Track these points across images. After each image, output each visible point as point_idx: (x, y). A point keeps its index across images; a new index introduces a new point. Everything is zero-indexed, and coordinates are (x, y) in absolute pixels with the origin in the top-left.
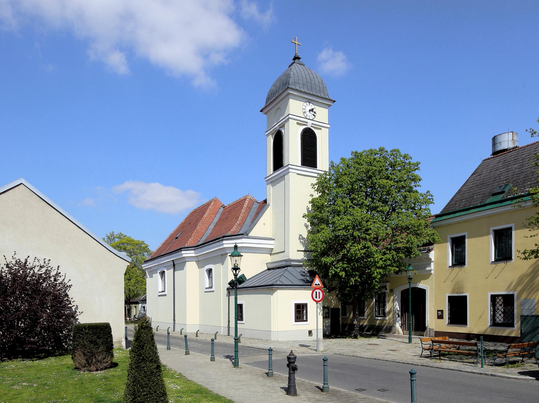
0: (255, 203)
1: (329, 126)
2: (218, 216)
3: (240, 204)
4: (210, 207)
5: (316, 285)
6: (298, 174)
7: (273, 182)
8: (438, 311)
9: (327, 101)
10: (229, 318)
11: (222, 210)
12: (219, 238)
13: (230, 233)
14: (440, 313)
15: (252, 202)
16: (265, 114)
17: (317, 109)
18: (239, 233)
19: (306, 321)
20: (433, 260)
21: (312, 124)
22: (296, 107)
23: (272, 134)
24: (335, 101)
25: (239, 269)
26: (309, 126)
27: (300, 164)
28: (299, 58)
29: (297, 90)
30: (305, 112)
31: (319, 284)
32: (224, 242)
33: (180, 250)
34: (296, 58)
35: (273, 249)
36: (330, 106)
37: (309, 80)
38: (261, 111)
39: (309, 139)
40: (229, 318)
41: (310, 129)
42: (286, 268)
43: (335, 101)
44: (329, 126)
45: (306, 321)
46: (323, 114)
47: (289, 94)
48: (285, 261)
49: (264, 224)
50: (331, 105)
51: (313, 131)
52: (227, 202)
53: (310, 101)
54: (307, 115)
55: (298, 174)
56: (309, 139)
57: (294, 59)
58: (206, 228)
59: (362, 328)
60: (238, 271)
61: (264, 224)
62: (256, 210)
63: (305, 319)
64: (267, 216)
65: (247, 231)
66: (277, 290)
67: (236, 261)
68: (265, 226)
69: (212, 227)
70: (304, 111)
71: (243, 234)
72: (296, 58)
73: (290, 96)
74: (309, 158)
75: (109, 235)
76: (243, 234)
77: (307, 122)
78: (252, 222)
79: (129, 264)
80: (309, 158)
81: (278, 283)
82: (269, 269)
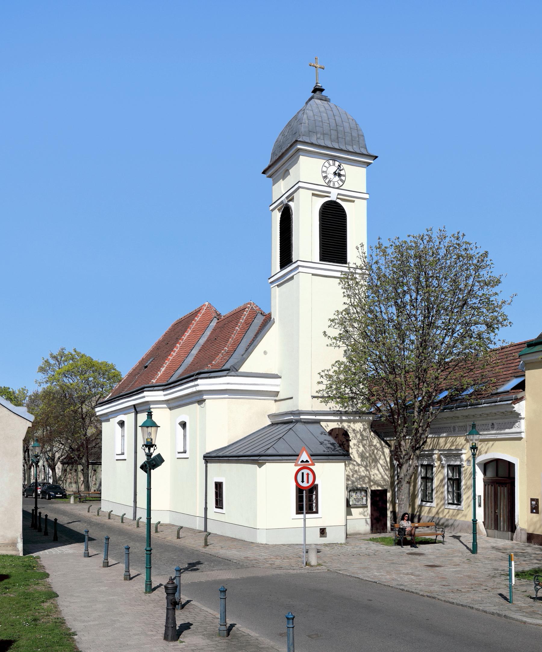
0: (259, 316)
1: (367, 196)
2: (208, 333)
3: (237, 315)
4: (200, 315)
5: (302, 461)
6: (313, 275)
7: (282, 282)
8: (532, 500)
9: (366, 158)
10: (206, 503)
11: (215, 321)
12: (193, 376)
13: (209, 368)
14: (534, 503)
15: (254, 314)
16: (270, 177)
17: (348, 170)
18: (224, 368)
19: (317, 512)
20: (523, 415)
21: (339, 194)
22: (309, 169)
23: (279, 210)
24: (376, 157)
25: (152, 446)
26: (333, 198)
27: (318, 261)
28: (322, 90)
29: (312, 144)
30: (325, 177)
31: (307, 461)
32: (199, 382)
33: (141, 390)
34: (318, 90)
35: (278, 392)
36: (369, 164)
37: (333, 124)
38: (264, 173)
39: (333, 219)
40: (206, 503)
41: (335, 202)
42: (291, 426)
43: (376, 157)
44: (367, 196)
45: (317, 512)
46: (356, 177)
47: (299, 150)
48: (292, 413)
49: (265, 353)
50: (372, 163)
51: (341, 206)
52: (225, 312)
53: (334, 159)
54: (330, 181)
55: (313, 275)
56: (333, 219)
57: (315, 91)
58: (185, 354)
59: (536, 504)
60: (152, 449)
61: (265, 353)
62: (257, 328)
63: (314, 510)
64: (271, 339)
65: (236, 364)
66: (265, 463)
67: (150, 434)
68: (265, 355)
69: (195, 352)
70: (324, 175)
71: (228, 370)
72: (318, 90)
73: (301, 153)
74: (333, 245)
75: (55, 353)
76: (228, 370)
77: (329, 193)
78: (247, 349)
79: (30, 425)
80: (333, 245)
81: (270, 452)
82: (273, 424)
